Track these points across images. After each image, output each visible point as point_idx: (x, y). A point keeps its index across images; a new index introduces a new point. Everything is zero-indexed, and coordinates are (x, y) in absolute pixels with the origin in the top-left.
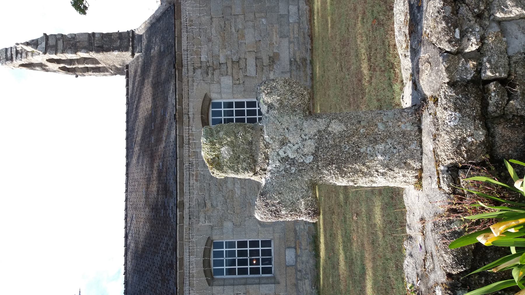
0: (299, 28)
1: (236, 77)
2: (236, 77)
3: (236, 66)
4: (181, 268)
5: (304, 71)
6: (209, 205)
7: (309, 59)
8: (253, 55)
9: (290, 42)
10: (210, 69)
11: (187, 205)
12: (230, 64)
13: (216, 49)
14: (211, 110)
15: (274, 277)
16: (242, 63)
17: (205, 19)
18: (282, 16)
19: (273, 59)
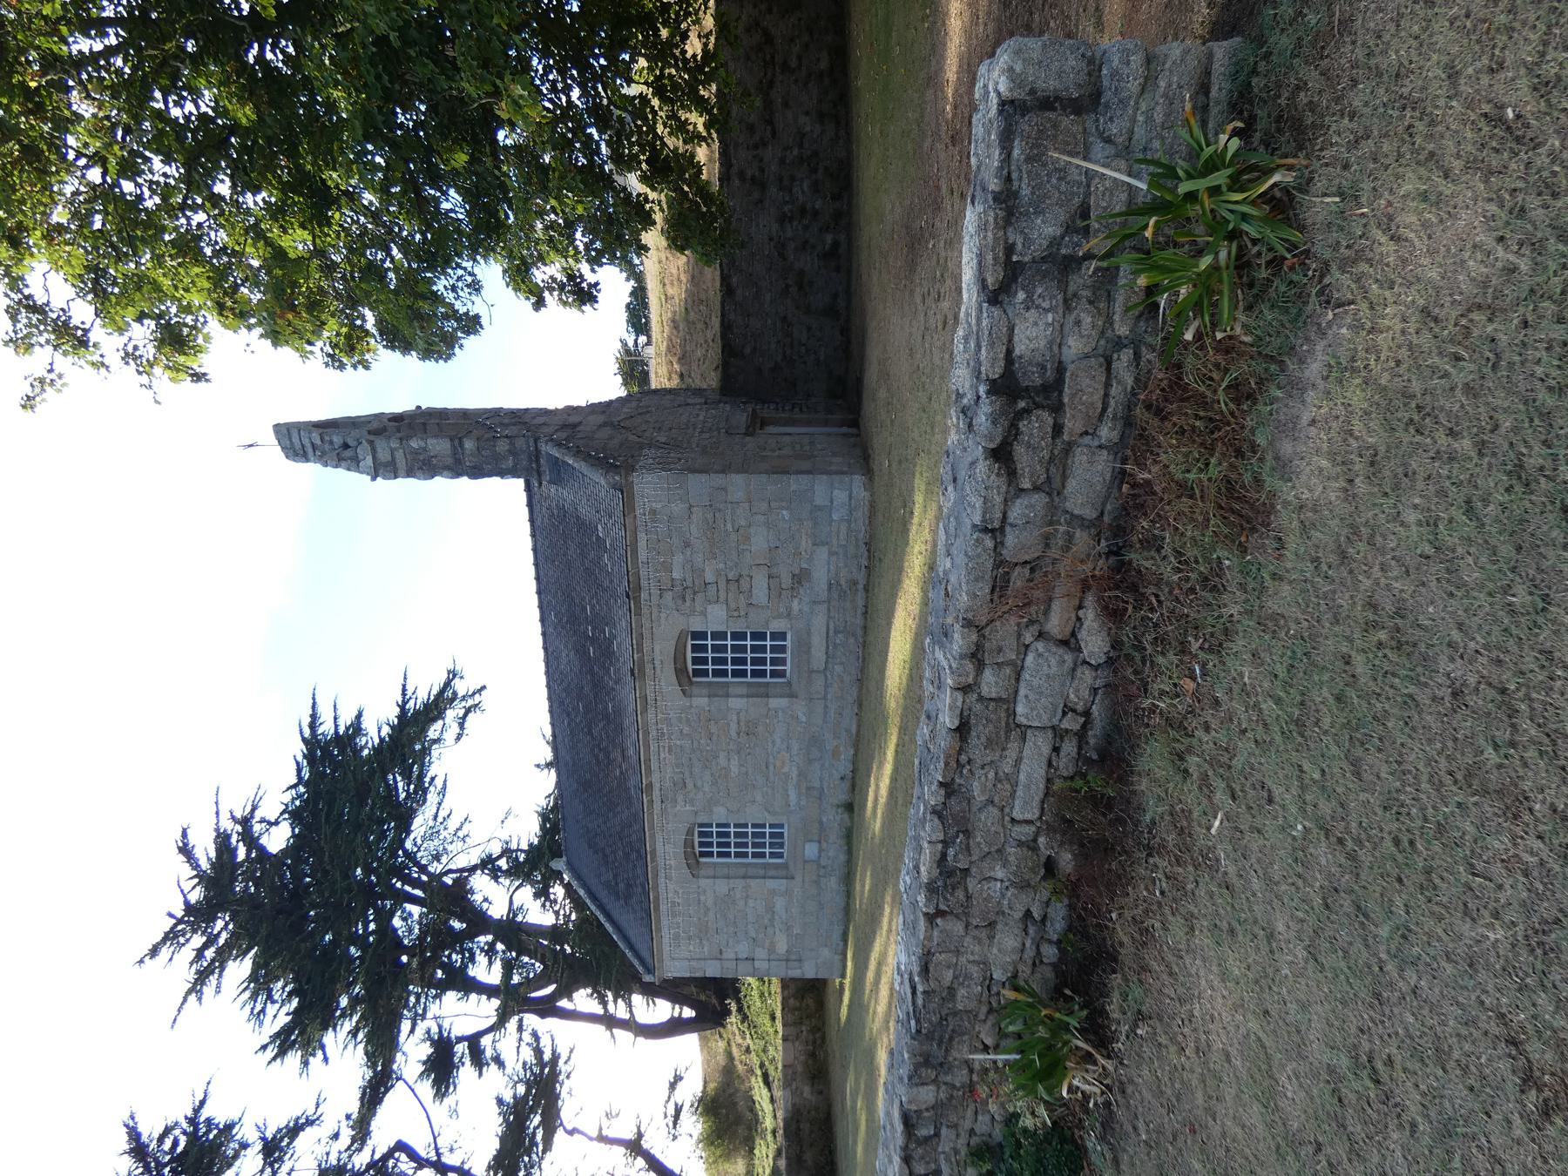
0: (849, 530)
1: (733, 605)
2: (733, 605)
3: (733, 586)
4: (653, 860)
5: (853, 601)
6: (690, 785)
7: (862, 583)
8: (764, 571)
9: (831, 554)
10: (688, 592)
11: (656, 786)
12: (722, 584)
13: (699, 558)
14: (690, 643)
15: (789, 683)
16: (744, 584)
17: (678, 508)
18: (819, 508)
19: (800, 578)
